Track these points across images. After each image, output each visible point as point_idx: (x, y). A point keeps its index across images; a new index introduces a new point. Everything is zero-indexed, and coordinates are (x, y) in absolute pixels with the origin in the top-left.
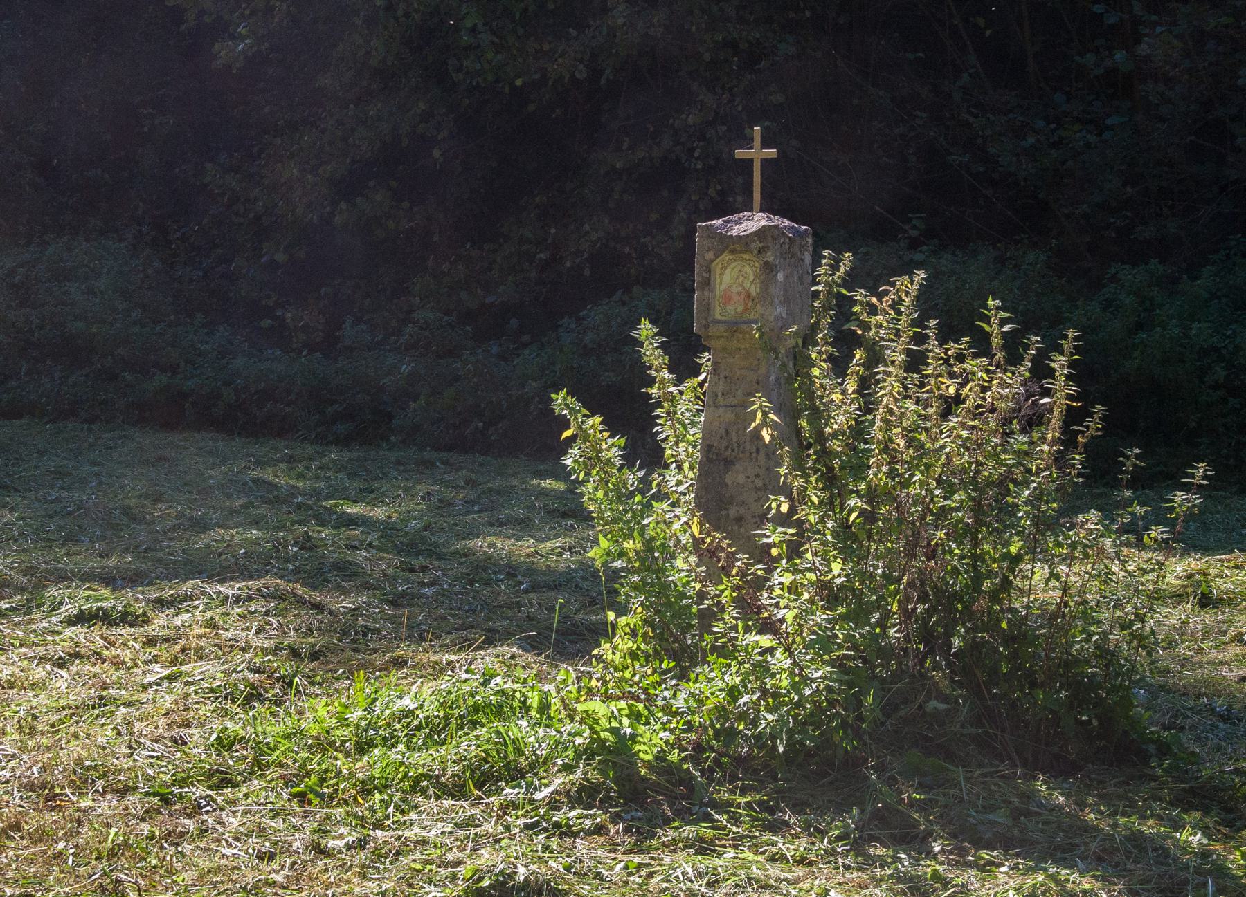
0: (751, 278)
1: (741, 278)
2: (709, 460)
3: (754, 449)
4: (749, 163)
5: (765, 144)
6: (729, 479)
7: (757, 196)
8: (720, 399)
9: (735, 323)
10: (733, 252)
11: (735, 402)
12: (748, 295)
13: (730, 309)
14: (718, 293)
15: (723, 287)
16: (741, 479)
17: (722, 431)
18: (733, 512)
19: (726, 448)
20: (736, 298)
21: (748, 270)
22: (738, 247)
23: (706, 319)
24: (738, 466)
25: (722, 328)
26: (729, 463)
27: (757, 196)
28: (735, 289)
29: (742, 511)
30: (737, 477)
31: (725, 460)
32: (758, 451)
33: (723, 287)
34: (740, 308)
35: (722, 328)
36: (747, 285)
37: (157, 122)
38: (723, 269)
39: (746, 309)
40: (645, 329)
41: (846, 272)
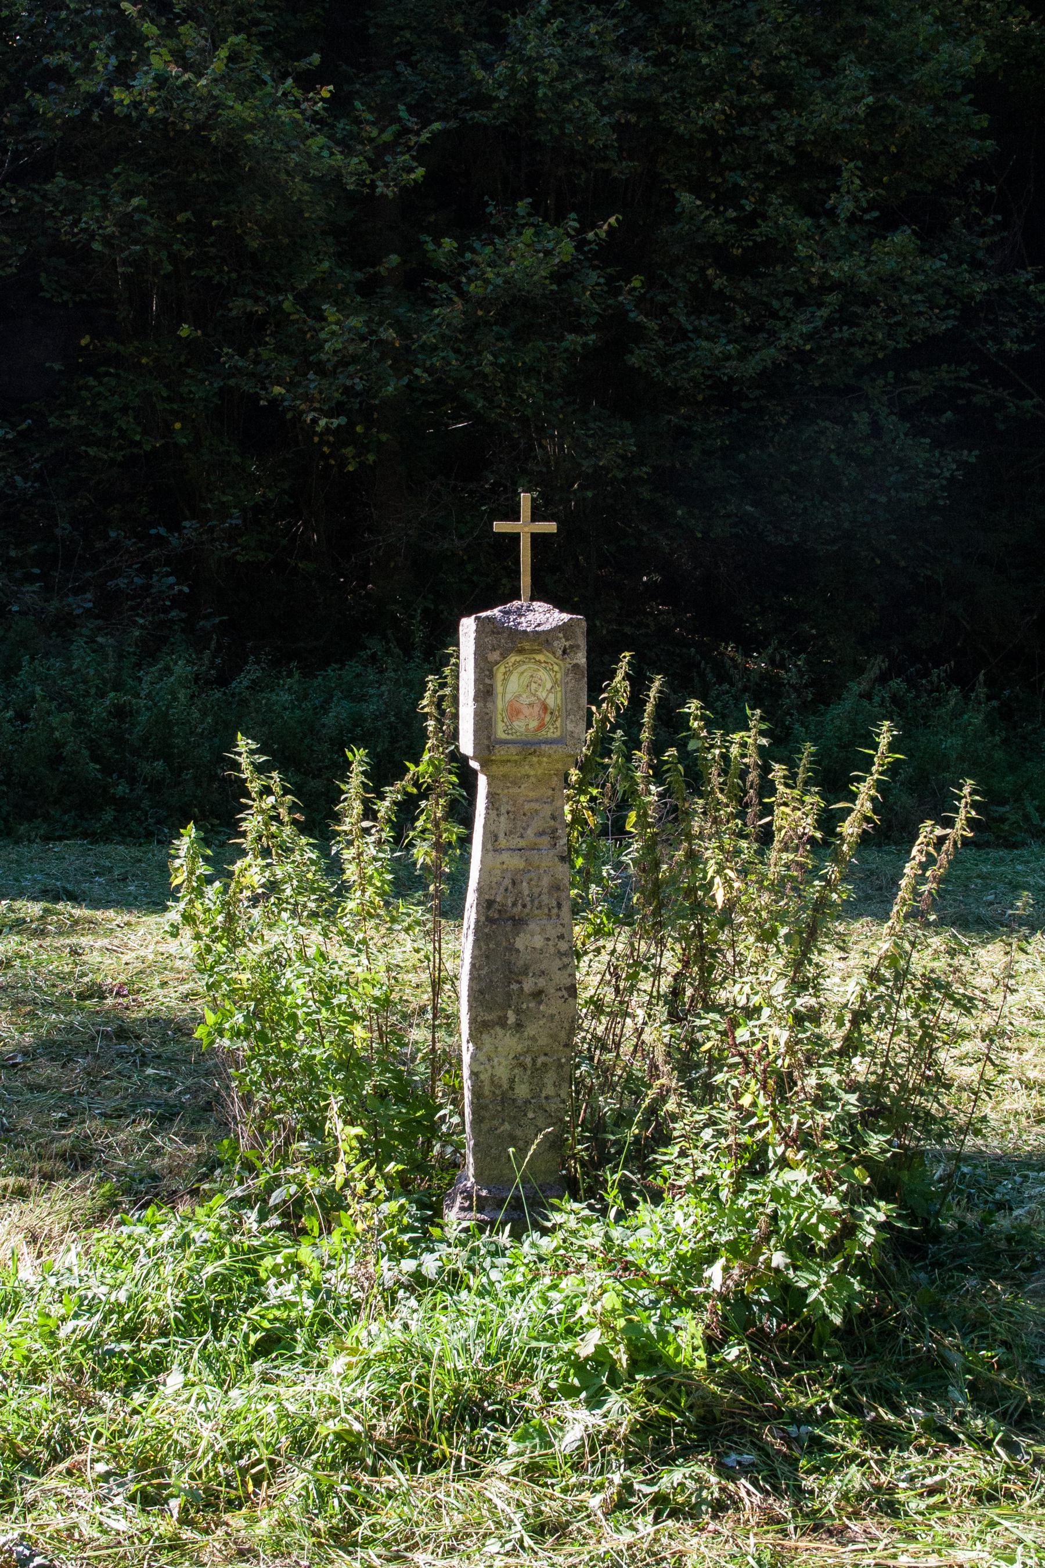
0: (549, 685)
1: (534, 686)
2: (490, 920)
3: (554, 904)
4: (515, 538)
5: (537, 516)
6: (520, 943)
7: (525, 581)
8: (503, 842)
9: (532, 744)
10: (521, 651)
11: (522, 843)
12: (545, 708)
13: (519, 725)
14: (500, 704)
15: (508, 696)
16: (538, 942)
17: (507, 882)
18: (528, 986)
19: (514, 904)
20: (526, 711)
21: (543, 674)
22: (527, 645)
23: (489, 738)
24: (532, 926)
25: (513, 750)
26: (519, 923)
27: (525, 581)
28: (525, 699)
29: (542, 982)
30: (531, 940)
31: (513, 918)
32: (559, 906)
33: (508, 696)
34: (534, 724)
35: (513, 750)
36: (542, 695)
37: (958, 146)
38: (508, 673)
39: (542, 726)
40: (968, 786)
41: (649, 688)
